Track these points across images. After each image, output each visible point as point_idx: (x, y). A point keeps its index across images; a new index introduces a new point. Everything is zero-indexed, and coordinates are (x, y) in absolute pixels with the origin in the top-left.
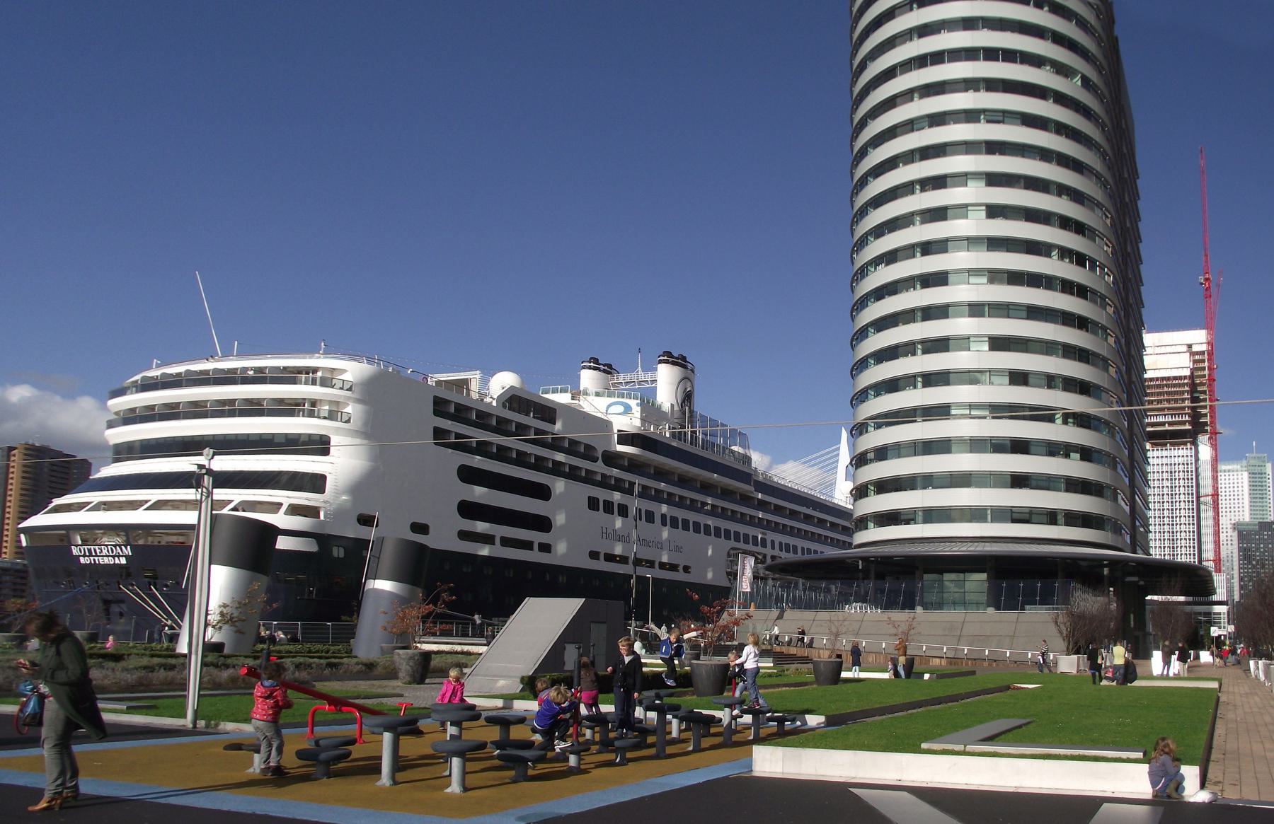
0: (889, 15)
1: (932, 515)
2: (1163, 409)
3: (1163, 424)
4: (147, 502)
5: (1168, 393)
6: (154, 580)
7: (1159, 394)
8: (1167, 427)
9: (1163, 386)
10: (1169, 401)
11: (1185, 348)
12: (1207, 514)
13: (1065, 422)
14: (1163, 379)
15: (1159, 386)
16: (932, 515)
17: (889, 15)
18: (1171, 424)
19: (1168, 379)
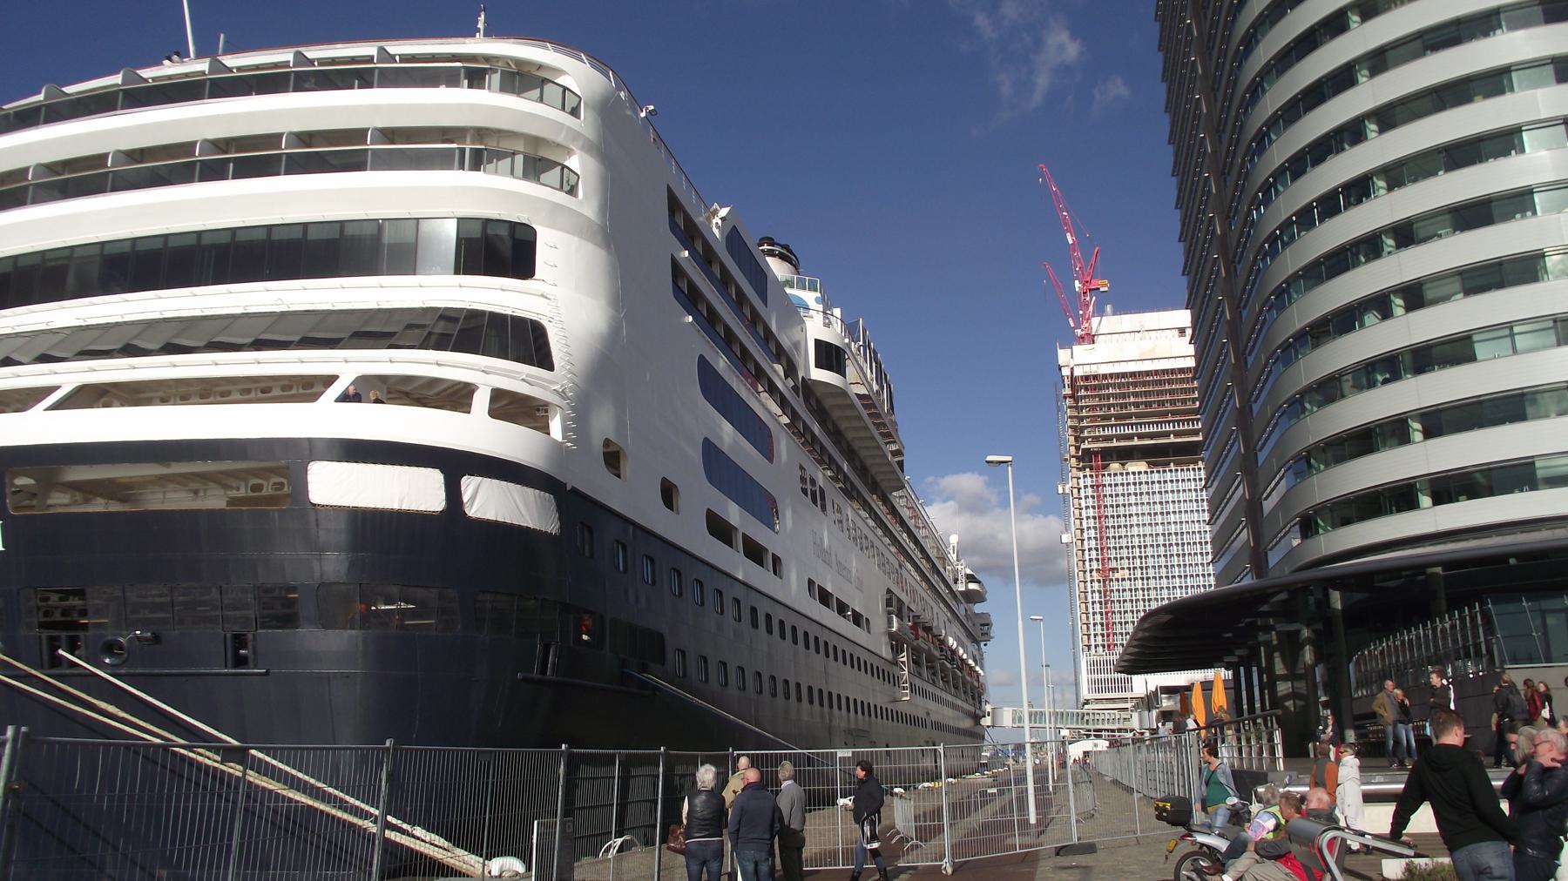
0: (1335, 25)
1: (1449, 487)
2: (1165, 414)
3: (1167, 434)
4: (50, 390)
5: (1171, 392)
6: (67, 629)
7: (1159, 393)
8: (1172, 439)
9: (1108, 386)
10: (1173, 402)
11: (1551, 324)
12: (934, 579)
13: (494, 413)
14: (1164, 372)
15: (1159, 383)
16: (1449, 487)
17: (1335, 25)
18: (1177, 434)
19: (1173, 371)
